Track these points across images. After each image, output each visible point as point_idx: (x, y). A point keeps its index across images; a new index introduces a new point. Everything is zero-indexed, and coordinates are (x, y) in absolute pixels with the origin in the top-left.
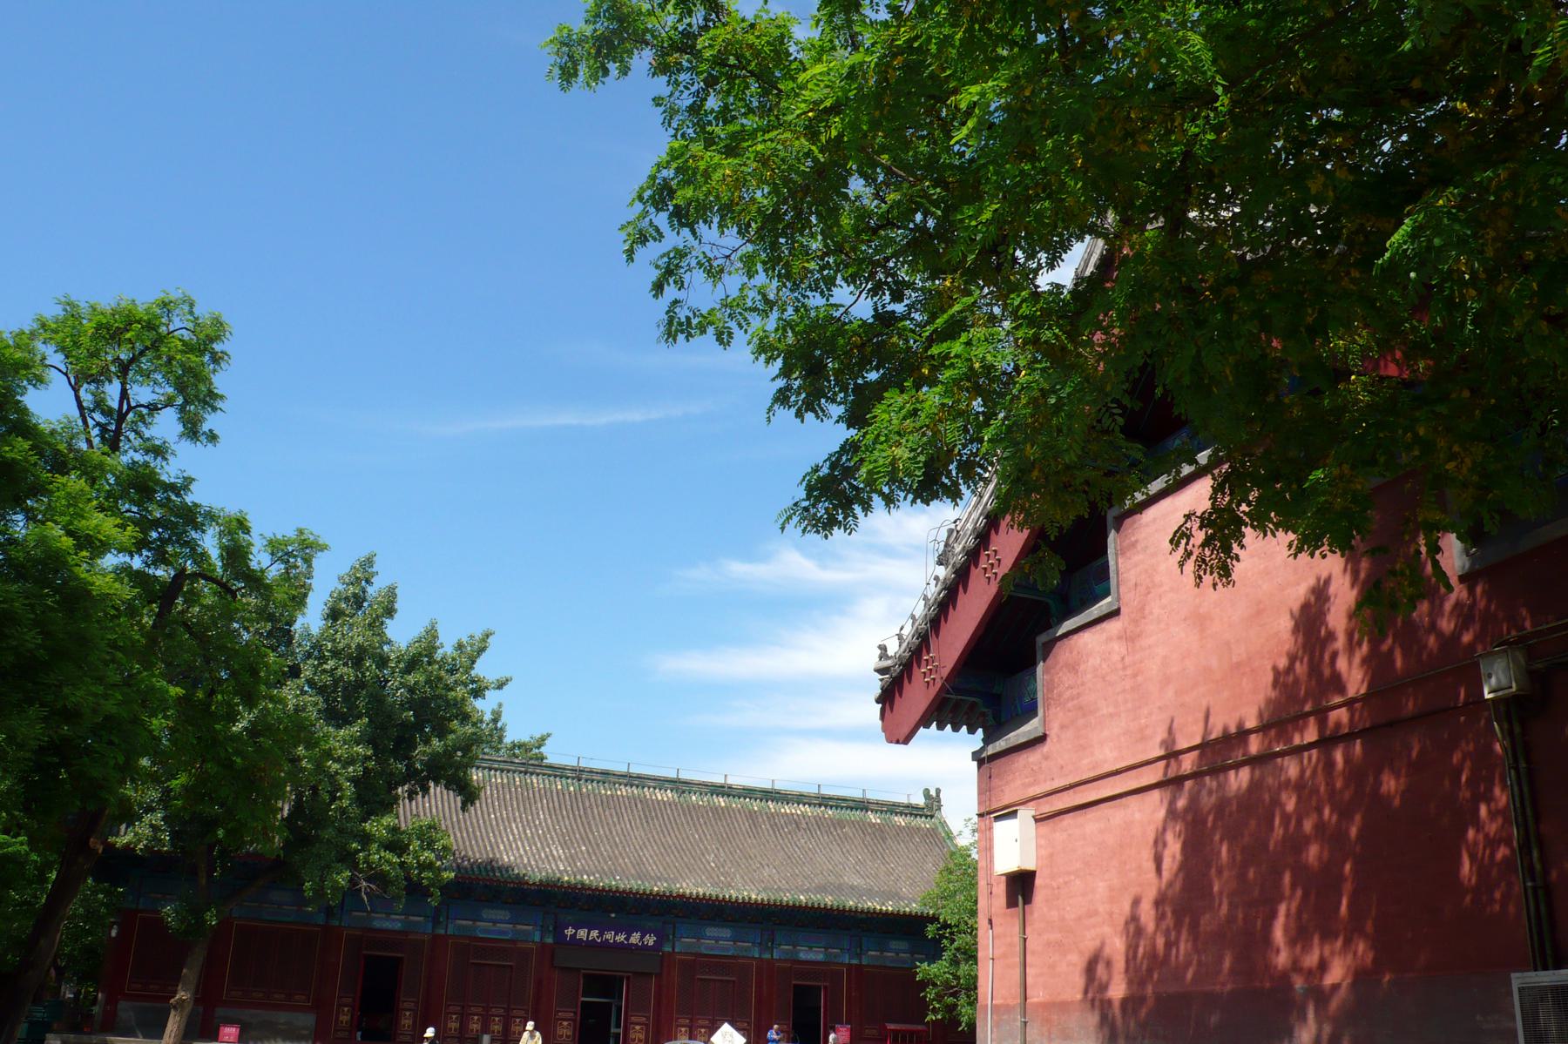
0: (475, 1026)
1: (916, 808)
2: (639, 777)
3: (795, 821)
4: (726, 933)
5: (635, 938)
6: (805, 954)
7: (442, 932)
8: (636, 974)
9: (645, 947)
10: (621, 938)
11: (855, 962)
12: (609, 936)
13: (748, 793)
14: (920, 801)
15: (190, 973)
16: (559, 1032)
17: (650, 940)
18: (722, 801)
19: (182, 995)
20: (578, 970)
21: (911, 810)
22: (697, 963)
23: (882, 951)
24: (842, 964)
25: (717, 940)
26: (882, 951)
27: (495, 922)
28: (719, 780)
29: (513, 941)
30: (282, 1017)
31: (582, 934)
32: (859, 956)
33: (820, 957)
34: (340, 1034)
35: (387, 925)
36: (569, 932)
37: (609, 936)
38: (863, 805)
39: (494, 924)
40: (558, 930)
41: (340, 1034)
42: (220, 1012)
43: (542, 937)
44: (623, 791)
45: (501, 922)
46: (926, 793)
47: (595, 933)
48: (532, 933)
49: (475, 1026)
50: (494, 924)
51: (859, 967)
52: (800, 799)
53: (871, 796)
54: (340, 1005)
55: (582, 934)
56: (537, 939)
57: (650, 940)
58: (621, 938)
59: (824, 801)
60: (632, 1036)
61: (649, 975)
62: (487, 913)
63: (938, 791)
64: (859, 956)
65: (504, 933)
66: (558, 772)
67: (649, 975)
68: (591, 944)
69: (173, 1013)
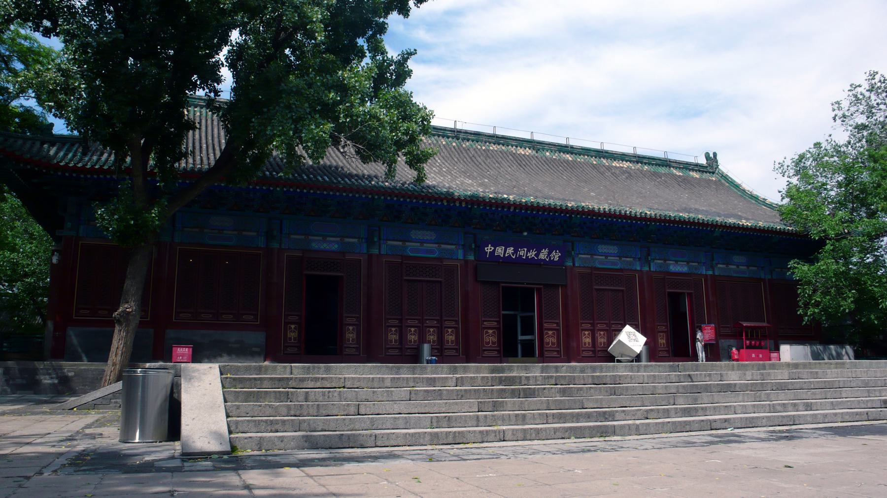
0: (413, 337)
1: (702, 166)
2: (503, 138)
3: (627, 172)
4: (613, 249)
5: (543, 255)
6: (674, 268)
7: (376, 251)
8: (546, 285)
9: (552, 262)
10: (532, 254)
11: (710, 273)
12: (522, 252)
13: (586, 151)
14: (703, 161)
15: (132, 287)
16: (486, 339)
17: (556, 256)
18: (569, 157)
19: (129, 307)
20: (498, 283)
21: (698, 168)
22: (592, 276)
23: (727, 264)
24: (701, 275)
25: (607, 256)
26: (727, 264)
27: (422, 242)
28: (563, 142)
29: (440, 259)
30: (233, 336)
31: (500, 251)
32: (713, 268)
33: (685, 269)
34: (289, 350)
35: (325, 246)
36: (489, 249)
37: (522, 252)
38: (666, 163)
39: (423, 244)
40: (479, 249)
41: (289, 350)
42: (171, 333)
43: (464, 255)
44: (493, 147)
45: (428, 242)
46: (707, 156)
47: (510, 250)
48: (457, 253)
49: (413, 337)
50: (423, 244)
51: (713, 276)
52: (623, 157)
53: (672, 157)
54: (286, 324)
55: (500, 251)
56: (461, 257)
57: (556, 256)
58: (532, 254)
59: (639, 159)
60: (546, 340)
61: (556, 286)
62: (416, 234)
63: (715, 154)
64: (713, 268)
65: (432, 252)
66: (442, 132)
67: (556, 286)
68: (507, 260)
69: (117, 328)
